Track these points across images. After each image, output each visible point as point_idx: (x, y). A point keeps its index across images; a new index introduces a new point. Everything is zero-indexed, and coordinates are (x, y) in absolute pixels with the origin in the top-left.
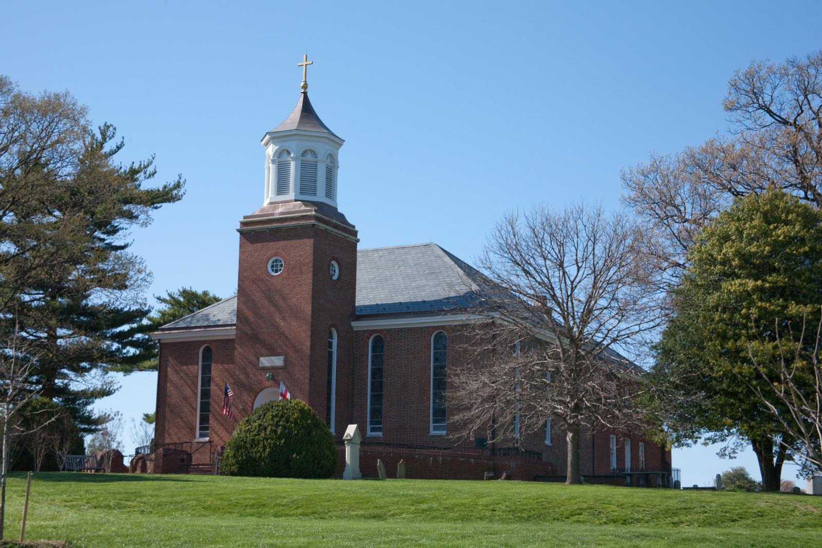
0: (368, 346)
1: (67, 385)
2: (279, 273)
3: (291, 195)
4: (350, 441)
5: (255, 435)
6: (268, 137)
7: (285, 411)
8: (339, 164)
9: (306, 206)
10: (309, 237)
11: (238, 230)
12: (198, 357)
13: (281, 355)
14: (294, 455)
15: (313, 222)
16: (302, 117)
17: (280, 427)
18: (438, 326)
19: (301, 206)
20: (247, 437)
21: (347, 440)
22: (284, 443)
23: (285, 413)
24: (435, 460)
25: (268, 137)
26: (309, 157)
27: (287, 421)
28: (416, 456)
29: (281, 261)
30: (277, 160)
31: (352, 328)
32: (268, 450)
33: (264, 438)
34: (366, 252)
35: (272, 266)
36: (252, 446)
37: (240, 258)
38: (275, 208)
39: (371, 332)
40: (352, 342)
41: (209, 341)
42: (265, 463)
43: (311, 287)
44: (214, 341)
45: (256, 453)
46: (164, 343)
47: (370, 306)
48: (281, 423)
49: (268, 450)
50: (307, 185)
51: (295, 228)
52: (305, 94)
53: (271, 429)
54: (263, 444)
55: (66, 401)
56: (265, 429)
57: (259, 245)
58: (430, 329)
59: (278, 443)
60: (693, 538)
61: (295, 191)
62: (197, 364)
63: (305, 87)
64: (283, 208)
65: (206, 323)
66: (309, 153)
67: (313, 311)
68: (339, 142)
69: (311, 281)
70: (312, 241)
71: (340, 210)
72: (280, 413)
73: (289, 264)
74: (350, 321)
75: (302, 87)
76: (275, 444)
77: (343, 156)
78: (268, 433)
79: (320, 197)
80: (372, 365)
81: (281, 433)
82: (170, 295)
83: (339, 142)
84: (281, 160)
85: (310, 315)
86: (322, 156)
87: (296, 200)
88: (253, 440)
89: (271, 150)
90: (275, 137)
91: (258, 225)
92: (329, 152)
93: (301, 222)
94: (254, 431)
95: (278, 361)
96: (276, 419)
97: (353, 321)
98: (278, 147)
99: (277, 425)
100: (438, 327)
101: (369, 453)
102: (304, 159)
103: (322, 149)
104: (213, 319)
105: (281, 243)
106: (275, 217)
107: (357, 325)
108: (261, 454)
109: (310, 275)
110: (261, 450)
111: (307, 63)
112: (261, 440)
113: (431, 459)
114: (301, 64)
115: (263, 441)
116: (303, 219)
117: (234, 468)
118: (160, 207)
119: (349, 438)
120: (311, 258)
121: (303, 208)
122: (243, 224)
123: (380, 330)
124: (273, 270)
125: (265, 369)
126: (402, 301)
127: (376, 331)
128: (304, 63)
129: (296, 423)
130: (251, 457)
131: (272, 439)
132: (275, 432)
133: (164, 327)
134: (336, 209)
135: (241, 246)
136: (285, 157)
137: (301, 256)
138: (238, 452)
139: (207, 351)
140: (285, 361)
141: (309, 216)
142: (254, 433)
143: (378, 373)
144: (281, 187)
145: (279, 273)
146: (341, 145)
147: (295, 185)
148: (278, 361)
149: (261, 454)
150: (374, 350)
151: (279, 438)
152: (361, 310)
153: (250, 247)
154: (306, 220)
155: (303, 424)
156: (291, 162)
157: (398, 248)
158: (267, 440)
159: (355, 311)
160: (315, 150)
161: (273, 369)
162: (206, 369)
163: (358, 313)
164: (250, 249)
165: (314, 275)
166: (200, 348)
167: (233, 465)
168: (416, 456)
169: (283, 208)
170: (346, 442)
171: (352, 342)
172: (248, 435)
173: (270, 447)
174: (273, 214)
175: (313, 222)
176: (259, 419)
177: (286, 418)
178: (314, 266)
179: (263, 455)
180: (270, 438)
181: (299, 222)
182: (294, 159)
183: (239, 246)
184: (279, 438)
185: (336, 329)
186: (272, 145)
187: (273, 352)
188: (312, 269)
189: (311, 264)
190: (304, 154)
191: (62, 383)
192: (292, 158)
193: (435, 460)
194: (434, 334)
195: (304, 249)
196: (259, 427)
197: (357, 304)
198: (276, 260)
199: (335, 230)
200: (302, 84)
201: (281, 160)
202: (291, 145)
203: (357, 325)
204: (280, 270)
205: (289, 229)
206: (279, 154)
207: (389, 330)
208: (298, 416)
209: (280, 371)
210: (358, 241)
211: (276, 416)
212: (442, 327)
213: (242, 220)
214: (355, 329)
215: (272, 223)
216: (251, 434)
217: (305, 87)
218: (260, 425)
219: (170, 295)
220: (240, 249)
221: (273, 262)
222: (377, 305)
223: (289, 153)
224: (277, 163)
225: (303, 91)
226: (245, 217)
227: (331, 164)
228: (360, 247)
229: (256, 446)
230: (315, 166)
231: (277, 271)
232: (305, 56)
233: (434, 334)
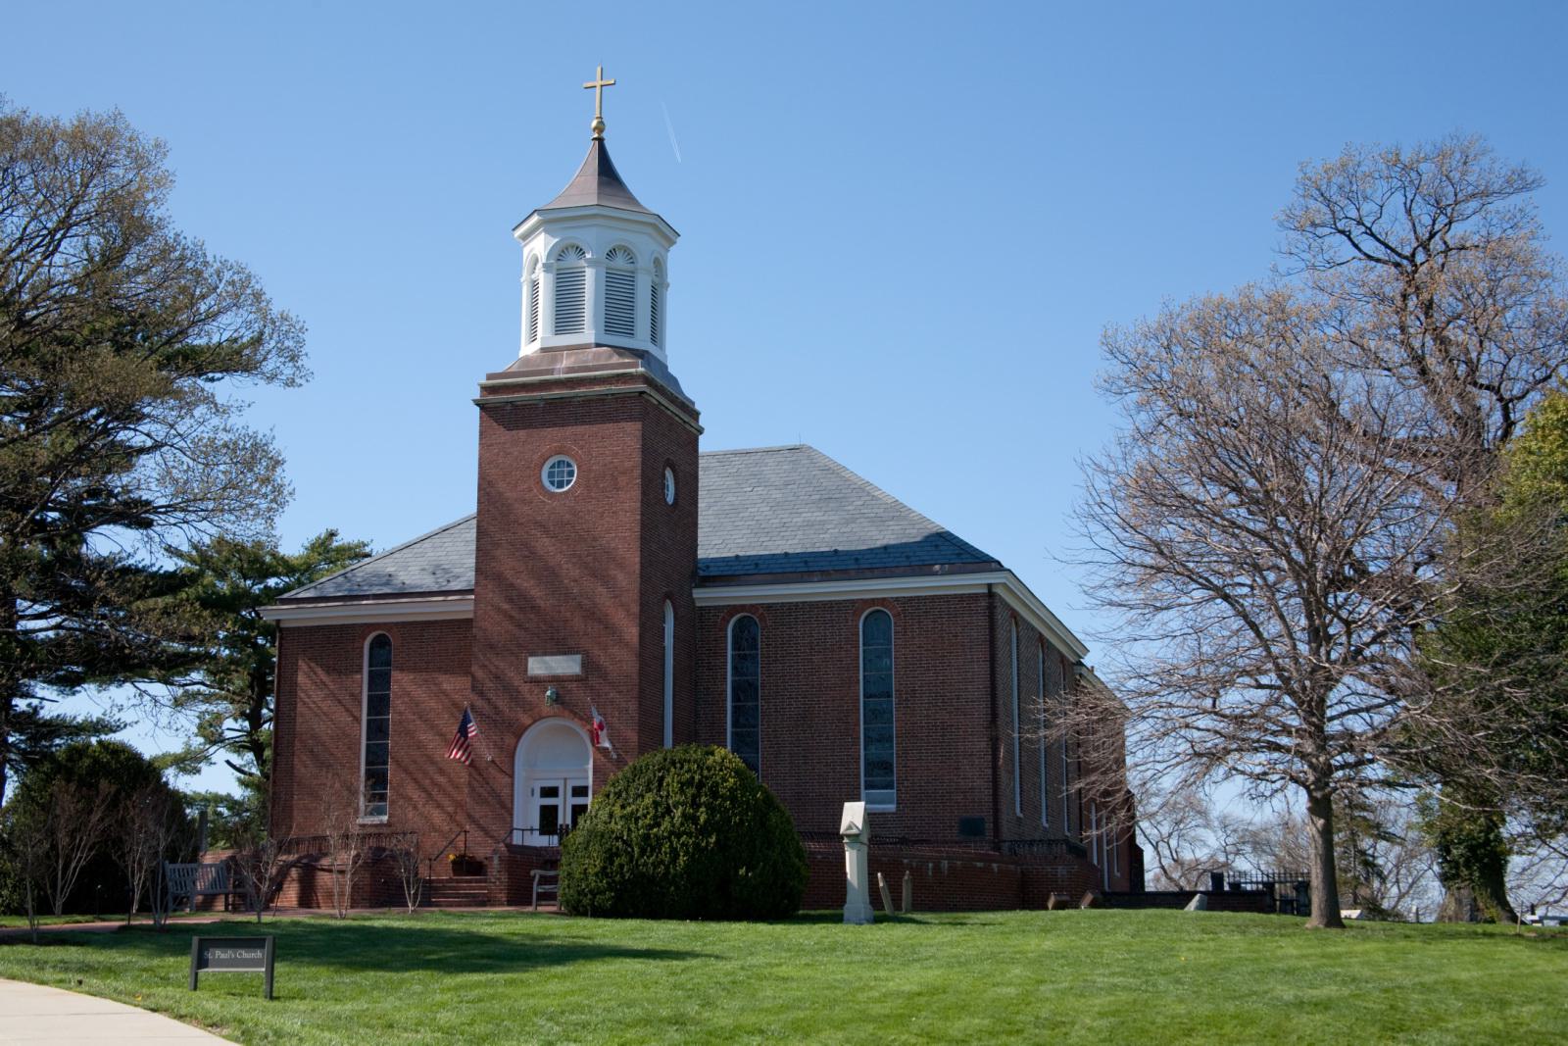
0: (726, 637)
1: (36, 710)
2: (566, 489)
3: (588, 334)
4: (855, 838)
5: (651, 827)
6: (535, 218)
7: (705, 772)
8: (669, 280)
9: (621, 355)
10: (631, 419)
11: (477, 403)
12: (362, 657)
13: (577, 653)
14: (742, 871)
15: (642, 387)
16: (600, 184)
17: (703, 809)
18: (873, 600)
19: (610, 357)
20: (629, 830)
21: (848, 836)
22: (715, 843)
23: (707, 778)
24: (937, 868)
25: (535, 218)
26: (620, 262)
27: (714, 794)
28: (905, 861)
29: (569, 465)
30: (555, 266)
31: (693, 601)
32: (682, 859)
33: (671, 833)
34: (724, 457)
35: (551, 475)
36: (643, 852)
37: (480, 459)
38: (554, 360)
39: (733, 610)
40: (699, 626)
41: (385, 624)
42: (677, 888)
43: (639, 517)
44: (397, 624)
45: (655, 865)
46: (288, 629)
47: (724, 560)
48: (703, 799)
49: (682, 859)
50: (617, 315)
51: (601, 399)
52: (600, 141)
53: (684, 815)
54: (671, 846)
55: (34, 739)
56: (668, 811)
57: (522, 433)
58: (854, 606)
59: (703, 844)
60: (1307, 1008)
61: (596, 328)
62: (360, 671)
63: (600, 128)
64: (573, 359)
65: (386, 590)
66: (620, 254)
67: (642, 564)
68: (667, 234)
69: (639, 504)
70: (639, 425)
71: (671, 370)
72: (697, 777)
73: (590, 471)
74: (691, 588)
75: (594, 129)
76: (697, 845)
77: (676, 260)
78: (677, 820)
79: (641, 341)
80: (733, 675)
81: (705, 822)
82: (195, 547)
83: (667, 234)
84: (563, 265)
85: (638, 572)
86: (644, 261)
87: (598, 345)
88: (646, 837)
89: (540, 246)
90: (552, 219)
91: (518, 392)
92: (655, 255)
93: (615, 388)
94: (645, 816)
95: (567, 665)
96: (690, 791)
97: (697, 587)
98: (557, 240)
99: (695, 805)
100: (873, 602)
101: (819, 857)
102: (612, 264)
103: (644, 245)
104: (397, 581)
105: (569, 430)
106: (556, 376)
107: (704, 596)
108: (667, 868)
109: (637, 493)
110: (667, 860)
111: (603, 83)
112: (664, 838)
113: (931, 865)
114: (589, 85)
115: (669, 838)
116: (618, 381)
117: (606, 899)
118: (219, 379)
119: (854, 831)
120: (637, 458)
121: (616, 359)
122: (485, 389)
123: (752, 606)
124: (552, 483)
125: (537, 681)
126: (840, 548)
127: (743, 608)
128: (599, 83)
129: (733, 799)
130: (643, 875)
131: (690, 835)
132: (695, 819)
133: (285, 596)
134: (666, 367)
135: (482, 434)
136: (572, 260)
137: (615, 454)
138: (612, 863)
139: (380, 643)
140: (584, 665)
141: (630, 374)
142: (647, 821)
143: (745, 690)
144: (565, 317)
145: (566, 489)
146: (672, 243)
147: (596, 315)
148: (567, 665)
149: (667, 868)
150: (736, 646)
151: (704, 831)
152: (708, 567)
153: (502, 435)
154: (625, 383)
155: (748, 802)
156: (587, 270)
157: (735, 454)
158: (679, 836)
159: (697, 568)
160: (630, 246)
161: (556, 680)
162: (380, 681)
163: (701, 573)
164: (503, 439)
165: (644, 493)
166: (364, 639)
167: (603, 892)
168: (905, 861)
169: (573, 359)
170: (846, 840)
171: (699, 626)
172: (632, 827)
173: (686, 853)
174: (551, 372)
175: (642, 387)
176: (649, 790)
177: (711, 789)
178: (644, 475)
179: (672, 871)
180: (684, 833)
181: (608, 387)
182: (592, 263)
183: (478, 434)
184: (704, 831)
185: (673, 603)
186: (542, 236)
187: (562, 648)
188: (639, 481)
189: (638, 472)
190: (611, 254)
191: (29, 705)
192: (588, 261)
193: (937, 868)
194: (739, 616)
195: (623, 441)
196: (656, 808)
197: (702, 554)
198: (559, 462)
199: (672, 408)
200: (594, 123)
201: (563, 265)
202: (586, 236)
203: (704, 596)
204: (569, 482)
205: (587, 402)
206: (559, 254)
207: (769, 607)
208: (735, 784)
209: (575, 685)
210: (701, 431)
211: (690, 782)
212: (883, 601)
213: (484, 381)
214: (698, 604)
215: (550, 389)
216: (640, 823)
217: (600, 128)
218: (656, 804)
219: (195, 547)
220: (481, 439)
221: (553, 467)
222: (737, 557)
223: (580, 252)
224: (555, 272)
225: (596, 136)
226: (490, 377)
227: (657, 280)
228: (705, 445)
229: (653, 850)
230: (630, 279)
231: (560, 485)
232: (599, 69)
233: (739, 616)
